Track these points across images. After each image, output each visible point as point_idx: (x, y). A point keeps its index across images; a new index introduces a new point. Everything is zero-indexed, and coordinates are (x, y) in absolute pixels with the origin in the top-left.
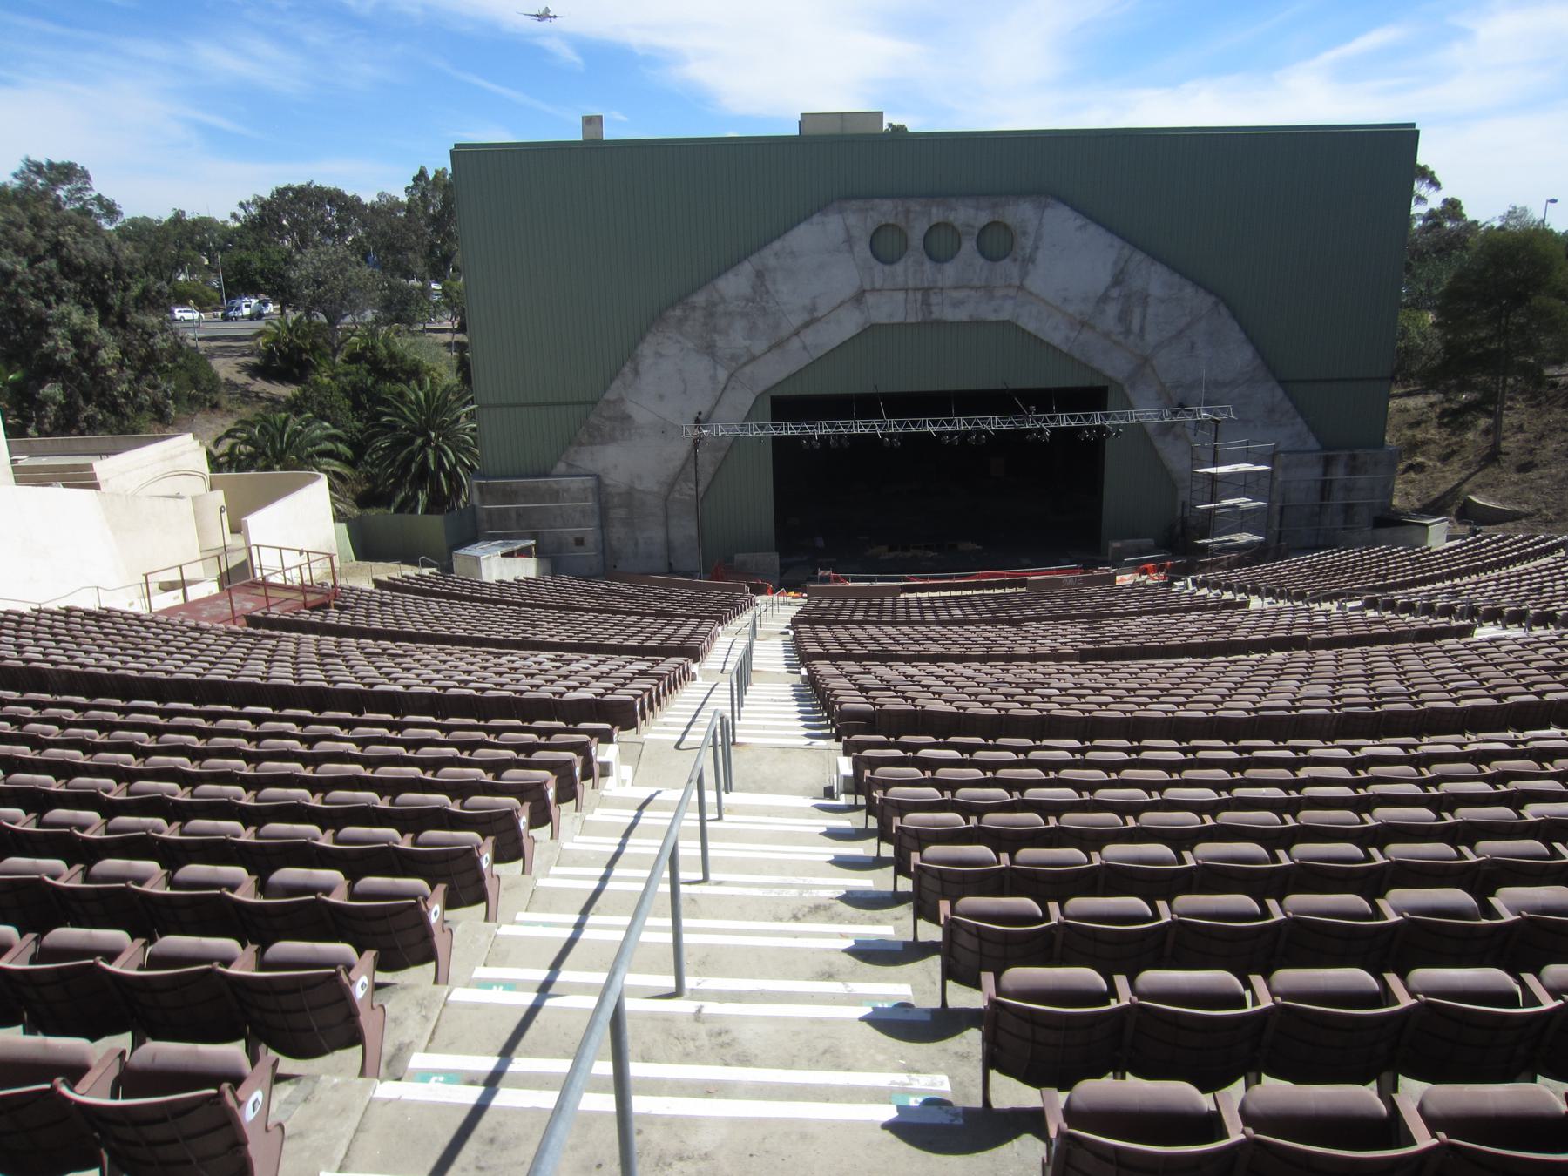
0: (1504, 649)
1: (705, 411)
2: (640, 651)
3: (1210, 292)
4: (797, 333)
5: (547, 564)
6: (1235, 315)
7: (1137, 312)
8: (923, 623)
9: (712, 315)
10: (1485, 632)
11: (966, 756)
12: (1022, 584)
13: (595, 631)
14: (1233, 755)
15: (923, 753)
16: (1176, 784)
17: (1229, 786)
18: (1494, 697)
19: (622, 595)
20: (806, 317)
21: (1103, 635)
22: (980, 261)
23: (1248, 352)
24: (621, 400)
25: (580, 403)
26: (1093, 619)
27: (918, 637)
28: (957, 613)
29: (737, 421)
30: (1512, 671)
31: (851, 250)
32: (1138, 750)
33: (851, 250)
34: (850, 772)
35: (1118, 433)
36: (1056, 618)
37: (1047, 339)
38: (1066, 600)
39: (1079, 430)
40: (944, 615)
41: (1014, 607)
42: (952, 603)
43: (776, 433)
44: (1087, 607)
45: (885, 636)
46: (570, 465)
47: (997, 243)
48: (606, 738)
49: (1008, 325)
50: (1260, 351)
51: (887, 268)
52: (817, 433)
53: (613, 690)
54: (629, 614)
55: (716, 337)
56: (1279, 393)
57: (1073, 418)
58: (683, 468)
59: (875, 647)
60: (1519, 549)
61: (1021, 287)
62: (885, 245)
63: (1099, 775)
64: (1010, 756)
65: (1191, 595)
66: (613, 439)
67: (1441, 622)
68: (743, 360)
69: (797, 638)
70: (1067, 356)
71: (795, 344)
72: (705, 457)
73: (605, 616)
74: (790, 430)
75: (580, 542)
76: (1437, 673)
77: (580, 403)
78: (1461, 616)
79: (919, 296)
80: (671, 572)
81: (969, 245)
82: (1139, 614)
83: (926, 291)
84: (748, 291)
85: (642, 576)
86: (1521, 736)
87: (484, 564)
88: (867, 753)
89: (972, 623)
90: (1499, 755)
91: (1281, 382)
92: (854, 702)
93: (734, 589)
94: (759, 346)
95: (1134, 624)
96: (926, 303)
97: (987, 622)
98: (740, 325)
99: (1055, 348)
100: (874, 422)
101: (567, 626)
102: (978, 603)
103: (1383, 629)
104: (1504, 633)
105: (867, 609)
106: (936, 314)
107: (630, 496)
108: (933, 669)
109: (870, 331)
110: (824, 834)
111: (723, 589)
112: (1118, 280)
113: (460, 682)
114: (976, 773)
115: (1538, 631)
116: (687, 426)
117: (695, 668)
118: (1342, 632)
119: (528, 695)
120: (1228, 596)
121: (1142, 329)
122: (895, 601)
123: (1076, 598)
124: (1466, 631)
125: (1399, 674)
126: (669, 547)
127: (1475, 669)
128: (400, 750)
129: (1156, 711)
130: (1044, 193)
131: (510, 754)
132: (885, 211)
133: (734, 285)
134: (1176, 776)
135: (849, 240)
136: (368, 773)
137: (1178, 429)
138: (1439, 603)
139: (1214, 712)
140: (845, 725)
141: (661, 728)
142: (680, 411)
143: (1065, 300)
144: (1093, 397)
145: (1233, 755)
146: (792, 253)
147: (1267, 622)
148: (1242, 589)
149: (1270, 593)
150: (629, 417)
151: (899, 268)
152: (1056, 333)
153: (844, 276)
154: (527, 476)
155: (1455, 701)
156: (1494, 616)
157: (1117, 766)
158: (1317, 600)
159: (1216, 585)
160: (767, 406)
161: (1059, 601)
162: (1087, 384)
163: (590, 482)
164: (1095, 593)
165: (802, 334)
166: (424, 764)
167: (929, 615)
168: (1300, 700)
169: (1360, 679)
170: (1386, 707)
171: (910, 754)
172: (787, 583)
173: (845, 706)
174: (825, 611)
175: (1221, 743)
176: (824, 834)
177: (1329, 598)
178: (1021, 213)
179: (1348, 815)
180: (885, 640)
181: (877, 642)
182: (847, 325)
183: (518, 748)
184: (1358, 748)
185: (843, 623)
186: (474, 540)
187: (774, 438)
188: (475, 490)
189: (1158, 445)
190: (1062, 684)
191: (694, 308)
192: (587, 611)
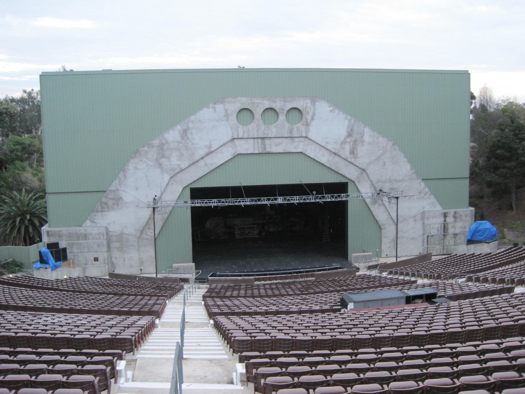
1: (158, 195)
9: (162, 149)
13: (106, 304)
14: (423, 353)
15: (280, 360)
16: (402, 368)
17: (396, 369)
20: (207, 151)
27: (265, 303)
32: (382, 353)
33: (228, 120)
34: (244, 371)
40: (277, 292)
43: (193, 205)
48: (120, 358)
58: (147, 223)
63: (365, 365)
64: (321, 359)
74: (198, 203)
76: (503, 309)
84: (179, 138)
92: (240, 336)
96: (264, 145)
107: (121, 237)
108: (275, 318)
112: (350, 135)
113: (42, 330)
114: (307, 368)
117: (157, 321)
120: (407, 278)
125: (487, 310)
127: (518, 307)
128: (16, 366)
129: (385, 334)
133: (172, 135)
134: (400, 364)
135: (227, 115)
140: (236, 346)
141: (146, 352)
143: (327, 143)
144: (341, 187)
146: (200, 121)
148: (413, 275)
149: (426, 276)
150: (121, 198)
152: (324, 158)
158: (446, 279)
160: (188, 193)
165: (205, 159)
166: (30, 372)
167: (270, 292)
168: (448, 325)
175: (416, 347)
182: (226, 154)
187: (192, 207)
190: (338, 323)
191: (153, 146)
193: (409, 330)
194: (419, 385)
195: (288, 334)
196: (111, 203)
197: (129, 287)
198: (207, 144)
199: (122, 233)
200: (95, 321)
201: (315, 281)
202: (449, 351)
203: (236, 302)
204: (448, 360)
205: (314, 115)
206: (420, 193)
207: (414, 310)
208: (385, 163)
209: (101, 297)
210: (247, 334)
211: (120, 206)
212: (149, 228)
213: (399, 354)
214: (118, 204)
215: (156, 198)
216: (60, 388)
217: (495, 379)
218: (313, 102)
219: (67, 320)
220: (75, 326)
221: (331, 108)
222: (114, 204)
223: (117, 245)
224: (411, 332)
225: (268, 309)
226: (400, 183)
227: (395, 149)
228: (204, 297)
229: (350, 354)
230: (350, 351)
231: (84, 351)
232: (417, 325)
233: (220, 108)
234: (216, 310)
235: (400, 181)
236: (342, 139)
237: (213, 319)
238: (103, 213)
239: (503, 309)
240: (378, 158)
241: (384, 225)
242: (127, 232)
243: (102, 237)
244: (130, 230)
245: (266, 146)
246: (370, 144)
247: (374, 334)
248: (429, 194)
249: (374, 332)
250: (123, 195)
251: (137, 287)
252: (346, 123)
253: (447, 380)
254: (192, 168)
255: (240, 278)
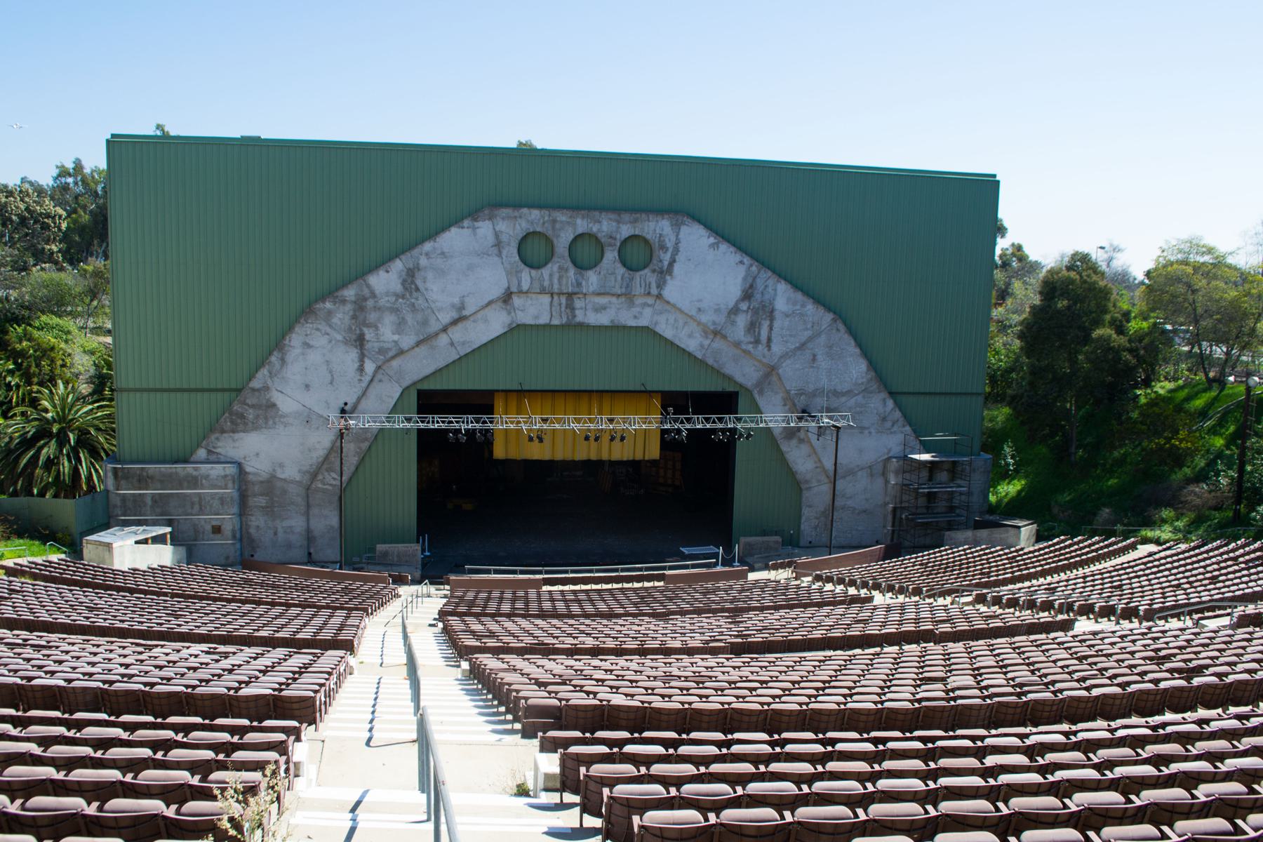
0: (1106, 641)
2: (295, 644)
3: (829, 309)
4: (445, 330)
5: (182, 550)
6: (851, 332)
7: (766, 324)
8: (572, 616)
10: (1084, 625)
11: (671, 751)
12: (661, 578)
13: (241, 622)
14: (869, 747)
17: (811, 779)
18: (1118, 685)
19: (262, 585)
20: (455, 315)
21: (748, 629)
22: (621, 270)
23: (863, 366)
24: (267, 388)
25: (223, 390)
26: (736, 613)
27: (570, 630)
28: (602, 607)
29: (382, 412)
30: (1095, 664)
31: (500, 255)
32: (728, 744)
33: (500, 255)
34: (556, 769)
35: (749, 436)
36: (699, 612)
37: (682, 346)
38: (704, 594)
39: (714, 431)
40: (589, 608)
41: (656, 600)
42: (595, 596)
43: (422, 426)
44: (726, 601)
45: (540, 630)
46: (210, 452)
47: (640, 256)
49: (648, 331)
50: (872, 365)
51: (534, 272)
52: (464, 427)
53: (208, 681)
54: (273, 604)
55: (366, 330)
56: (890, 403)
57: (707, 420)
58: (327, 457)
59: (529, 640)
60: (1096, 550)
61: (659, 296)
62: (533, 250)
63: (747, 768)
64: (658, 750)
65: (820, 590)
66: (256, 428)
67: (1044, 616)
68: (391, 354)
69: (447, 630)
70: (702, 363)
71: (443, 339)
72: (350, 447)
73: (248, 607)
74: (436, 423)
75: (217, 530)
76: (1060, 664)
77: (223, 390)
78: (1060, 611)
79: (563, 300)
80: (311, 561)
81: (611, 255)
82: (777, 608)
83: (570, 296)
84: (399, 288)
85: (280, 566)
86: (1074, 728)
87: (116, 552)
88: (574, 749)
89: (618, 616)
90: (1054, 748)
91: (891, 394)
92: (539, 698)
93: (377, 580)
94: (407, 341)
95: (773, 618)
96: (570, 307)
97: (634, 615)
98: (388, 321)
99: (690, 354)
100: (521, 418)
101: (212, 617)
102: (621, 597)
103: (997, 623)
104: (1097, 627)
105: (513, 601)
106: (580, 317)
107: (271, 485)
109: (516, 329)
110: (546, 833)
111: (365, 580)
112: (747, 295)
115: (1126, 624)
116: (333, 415)
117: (351, 660)
118: (963, 626)
119: (158, 688)
120: (852, 591)
121: (769, 340)
122: (539, 594)
123: (714, 592)
124: (1066, 626)
125: (1028, 665)
126: (310, 537)
129: (790, 704)
130: (680, 213)
131: (146, 752)
132: (533, 219)
133: (385, 281)
135: (498, 245)
136: (60, 776)
137: (802, 434)
138: (1041, 597)
139: (807, 704)
140: (540, 722)
142: (321, 403)
143: (700, 309)
144: (724, 402)
145: (869, 747)
146: (443, 253)
147: (895, 616)
149: (891, 588)
150: (274, 405)
151: (545, 272)
152: (692, 342)
153: (492, 278)
154: (164, 462)
155: (1088, 689)
156: (1087, 610)
157: (707, 760)
159: (841, 581)
161: (697, 595)
162: (719, 389)
163: (231, 470)
164: (731, 588)
165: (450, 331)
169: (966, 675)
170: (1031, 696)
171: (615, 750)
172: (431, 573)
173: (530, 702)
174: (472, 604)
175: (854, 735)
176: (546, 833)
177: (943, 594)
178: (657, 228)
179: (982, 805)
180: (538, 633)
181: (531, 635)
182: (495, 324)
183: (155, 745)
184: (1027, 736)
185: (493, 616)
186: (106, 526)
187: (420, 431)
188: (110, 474)
189: (784, 448)
191: (344, 302)
192: (229, 601)
193: (841, 699)
194: (856, 816)
195: (632, 696)
196: (251, 414)
197: (297, 590)
198: (456, 300)
199: (272, 478)
200: (196, 656)
201: (667, 589)
202: (918, 745)
203: (494, 627)
204: (916, 764)
205: (676, 250)
206: (884, 419)
207: (850, 660)
208: (814, 356)
209: (198, 606)
210: (550, 693)
211: (271, 422)
212: (329, 470)
213: (818, 748)
214: (266, 419)
215: (347, 408)
216: (118, 797)
217: (1207, 796)
218: (677, 226)
219: (125, 656)
220: (156, 667)
221: (712, 240)
222: (257, 417)
223: (262, 501)
224: (845, 704)
225: (575, 642)
226: (843, 399)
227: (838, 330)
228: (443, 614)
229: (719, 744)
230: (719, 736)
231: (173, 719)
232: (889, 687)
233: (485, 228)
234: (472, 642)
235: (843, 394)
236: (731, 305)
237: (470, 660)
238: (236, 436)
239: (1060, 664)
240: (802, 346)
241: (807, 482)
242: (282, 476)
243: (230, 485)
244: (291, 472)
245: (577, 312)
246: (787, 316)
247: (769, 704)
248: (900, 423)
249: (807, 700)
250: (277, 398)
251: (290, 588)
252: (741, 271)
253: (768, 812)
254: (422, 350)
255: (538, 576)
